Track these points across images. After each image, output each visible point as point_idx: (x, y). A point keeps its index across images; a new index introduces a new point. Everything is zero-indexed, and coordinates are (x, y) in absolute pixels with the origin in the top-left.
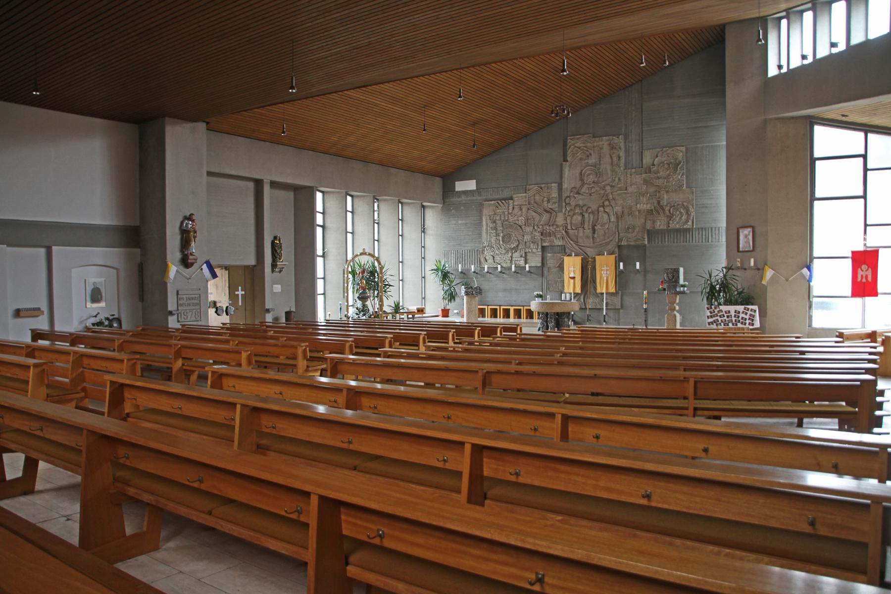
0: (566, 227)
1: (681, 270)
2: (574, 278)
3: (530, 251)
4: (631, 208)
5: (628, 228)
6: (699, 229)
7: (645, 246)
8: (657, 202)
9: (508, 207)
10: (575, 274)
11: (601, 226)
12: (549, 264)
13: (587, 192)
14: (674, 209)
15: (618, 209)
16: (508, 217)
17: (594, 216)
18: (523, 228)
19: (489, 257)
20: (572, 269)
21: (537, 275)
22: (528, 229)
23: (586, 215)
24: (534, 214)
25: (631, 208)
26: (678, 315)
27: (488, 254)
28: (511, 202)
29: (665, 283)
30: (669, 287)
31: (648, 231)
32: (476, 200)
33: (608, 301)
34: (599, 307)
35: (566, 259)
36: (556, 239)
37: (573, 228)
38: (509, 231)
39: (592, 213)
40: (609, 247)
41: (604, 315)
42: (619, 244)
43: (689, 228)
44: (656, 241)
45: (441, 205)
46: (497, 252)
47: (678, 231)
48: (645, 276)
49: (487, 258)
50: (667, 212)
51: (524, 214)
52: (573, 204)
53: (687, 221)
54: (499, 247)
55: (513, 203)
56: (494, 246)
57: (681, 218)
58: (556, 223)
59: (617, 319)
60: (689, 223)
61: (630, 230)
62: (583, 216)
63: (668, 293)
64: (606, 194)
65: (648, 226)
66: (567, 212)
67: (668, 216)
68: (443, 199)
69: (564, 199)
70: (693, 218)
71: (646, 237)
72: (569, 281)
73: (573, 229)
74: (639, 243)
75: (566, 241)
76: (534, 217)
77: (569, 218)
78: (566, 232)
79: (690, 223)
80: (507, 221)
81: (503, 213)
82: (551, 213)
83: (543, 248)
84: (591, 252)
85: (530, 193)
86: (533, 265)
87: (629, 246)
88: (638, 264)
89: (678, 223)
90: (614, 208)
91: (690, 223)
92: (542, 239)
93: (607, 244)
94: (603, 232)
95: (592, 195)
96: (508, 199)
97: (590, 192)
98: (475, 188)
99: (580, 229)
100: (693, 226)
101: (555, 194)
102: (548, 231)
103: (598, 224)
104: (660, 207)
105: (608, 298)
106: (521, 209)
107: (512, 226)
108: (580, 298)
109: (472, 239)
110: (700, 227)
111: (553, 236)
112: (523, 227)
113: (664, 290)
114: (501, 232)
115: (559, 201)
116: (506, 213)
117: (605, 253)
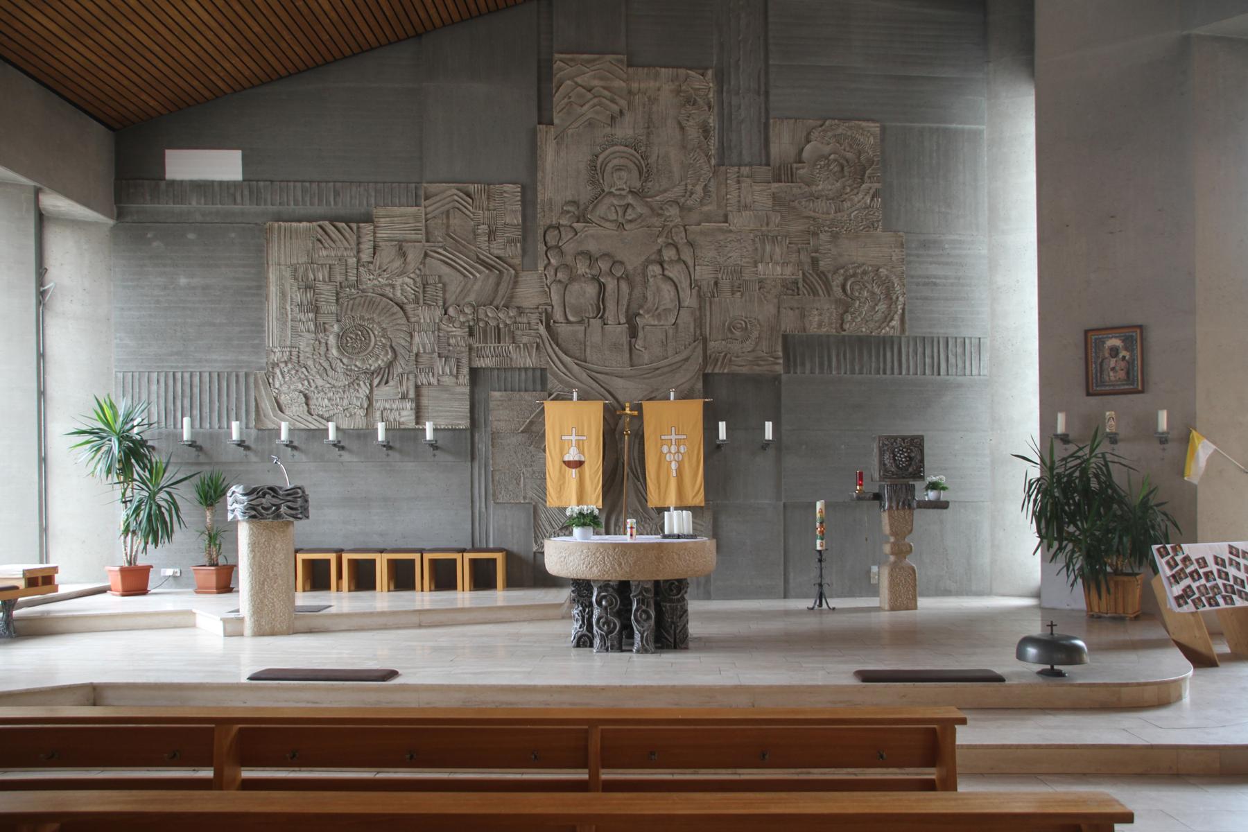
2: (579, 464)
3: (434, 381)
6: (915, 339)
10: (581, 452)
17: (632, 287)
18: (410, 313)
22: (425, 315)
24: (445, 270)
25: (739, 271)
28: (367, 228)
31: (785, 338)
37: (571, 319)
38: (362, 318)
44: (808, 366)
47: (862, 342)
49: (283, 399)
50: (837, 291)
51: (411, 267)
52: (569, 248)
53: (887, 318)
54: (326, 365)
56: (310, 363)
60: (893, 323)
65: (789, 323)
72: (562, 476)
73: (568, 322)
76: (445, 279)
84: (626, 390)
87: (733, 377)
90: (692, 270)
92: (471, 349)
100: (903, 330)
102: (493, 323)
104: (817, 275)
112: (409, 307)
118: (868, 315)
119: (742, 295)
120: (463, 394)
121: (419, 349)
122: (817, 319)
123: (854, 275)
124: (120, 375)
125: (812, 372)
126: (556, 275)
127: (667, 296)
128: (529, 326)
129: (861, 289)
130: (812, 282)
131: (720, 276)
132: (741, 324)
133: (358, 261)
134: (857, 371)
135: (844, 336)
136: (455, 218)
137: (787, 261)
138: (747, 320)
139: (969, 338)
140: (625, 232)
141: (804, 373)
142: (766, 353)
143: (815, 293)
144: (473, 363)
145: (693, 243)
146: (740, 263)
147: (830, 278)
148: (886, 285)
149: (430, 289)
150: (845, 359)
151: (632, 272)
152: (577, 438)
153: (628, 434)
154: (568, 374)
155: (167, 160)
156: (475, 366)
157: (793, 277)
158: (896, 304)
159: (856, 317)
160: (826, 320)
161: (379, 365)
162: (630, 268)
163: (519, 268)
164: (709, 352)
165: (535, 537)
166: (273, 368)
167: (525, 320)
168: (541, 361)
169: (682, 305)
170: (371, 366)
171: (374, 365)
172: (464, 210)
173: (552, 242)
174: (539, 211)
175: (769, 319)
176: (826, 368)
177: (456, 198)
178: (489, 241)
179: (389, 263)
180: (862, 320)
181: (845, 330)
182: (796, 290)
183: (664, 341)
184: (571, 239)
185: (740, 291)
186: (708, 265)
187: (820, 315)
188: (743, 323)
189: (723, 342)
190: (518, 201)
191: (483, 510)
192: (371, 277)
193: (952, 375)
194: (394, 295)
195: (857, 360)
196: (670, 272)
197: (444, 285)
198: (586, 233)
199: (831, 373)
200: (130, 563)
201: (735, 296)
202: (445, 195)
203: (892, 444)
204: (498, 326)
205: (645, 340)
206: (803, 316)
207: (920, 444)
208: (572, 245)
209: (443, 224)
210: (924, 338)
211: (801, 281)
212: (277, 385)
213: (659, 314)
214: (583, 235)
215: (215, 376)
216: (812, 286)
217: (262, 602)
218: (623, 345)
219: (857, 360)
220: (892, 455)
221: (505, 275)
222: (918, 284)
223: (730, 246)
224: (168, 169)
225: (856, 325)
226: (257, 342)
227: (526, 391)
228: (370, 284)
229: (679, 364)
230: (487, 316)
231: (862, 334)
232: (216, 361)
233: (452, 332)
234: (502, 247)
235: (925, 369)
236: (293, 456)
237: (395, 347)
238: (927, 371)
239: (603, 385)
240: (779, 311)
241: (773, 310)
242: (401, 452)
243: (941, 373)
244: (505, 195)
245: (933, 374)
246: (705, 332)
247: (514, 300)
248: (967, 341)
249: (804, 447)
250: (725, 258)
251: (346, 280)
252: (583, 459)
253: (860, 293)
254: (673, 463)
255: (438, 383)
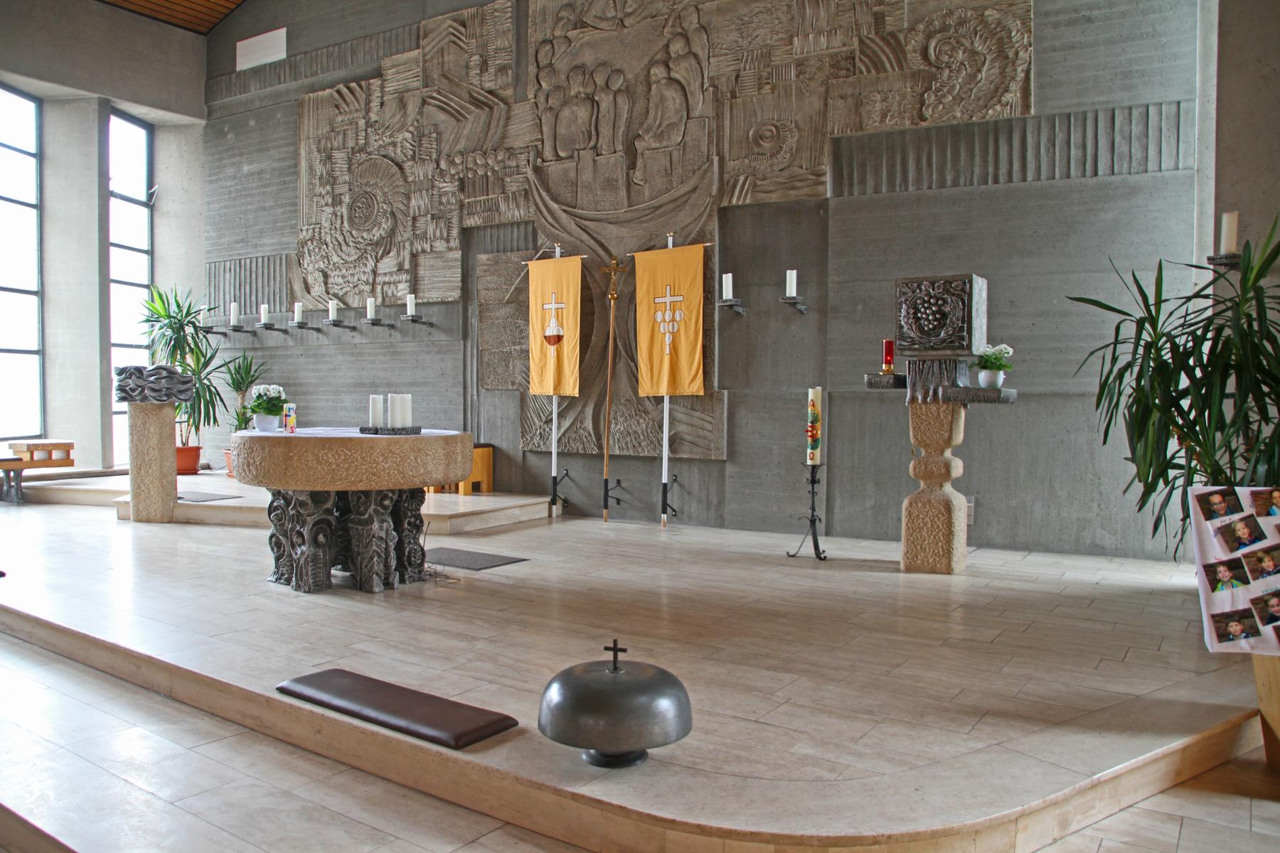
0: (539, 154)
1: (980, 287)
2: (559, 339)
3: (427, 247)
4: (766, 55)
5: (759, 137)
6: (1051, 119)
7: (823, 204)
8: (870, 19)
9: (368, 102)
10: (561, 325)
11: (659, 137)
12: (483, 293)
13: (611, 13)
14: (946, 41)
15: (720, 66)
16: (366, 137)
17: (633, 102)
18: (408, 171)
19: (315, 280)
20: (553, 306)
21: (448, 331)
22: (418, 172)
23: (605, 101)
24: (442, 117)
25: (766, 55)
26: (961, 505)
27: (312, 265)
28: (376, 83)
29: (903, 349)
30: (920, 368)
31: (836, 143)
32: (287, 92)
33: (682, 428)
34: (653, 454)
35: (535, 267)
36: (507, 199)
37: (562, 154)
38: (367, 184)
39: (628, 91)
40: (685, 217)
41: (665, 485)
42: (725, 204)
43: (1010, 121)
44: (870, 182)
45: (203, 122)
46: (335, 259)
47: (958, 134)
48: (823, 328)
49: (310, 280)
50: (915, 61)
51: (410, 120)
52: (562, 64)
53: (999, 90)
54: (341, 239)
55: (382, 87)
56: (328, 239)
57: (972, 78)
58: (510, 142)
59: (715, 501)
60: (1008, 97)
61: (766, 145)
62: (595, 104)
63: (914, 399)
64: (675, 14)
65: (837, 124)
66: (542, 99)
67: (915, 75)
68: (206, 102)
69: (531, 51)
70: (1027, 72)
71: (827, 168)
72: (543, 353)
73: (558, 158)
74: (802, 192)
75: (536, 205)
76: (442, 127)
77: (547, 119)
78: (537, 170)
79: (1014, 96)
80: (361, 150)
81: (353, 122)
82: (491, 108)
83: (467, 234)
84: (619, 239)
85: (429, 45)
86: (434, 296)
87: (760, 209)
88: (792, 276)
89: (958, 99)
90: (705, 64)
91: (1014, 96)
92: (462, 206)
93: (680, 203)
94: (664, 162)
95: (627, 23)
96: (367, 77)
97: (620, 15)
98: (283, 55)
99: (582, 152)
100: (1026, 106)
101: (502, 42)
102: (481, 172)
103: (648, 131)
104: (883, 39)
105: (679, 416)
106: (402, 104)
107: (376, 165)
108: (579, 419)
109: (275, 222)
110: (1073, 110)
111: (498, 191)
112: (408, 165)
113: (900, 382)
114: (345, 188)
115: (518, 63)
116: (362, 123)
117: (670, 240)
118: (964, 90)
119: (773, 89)
120: (455, 260)
121: (415, 212)
122: (878, 106)
123: (944, 28)
124: (208, 265)
125: (877, 190)
126: (547, 102)
127: (671, 107)
128: (518, 170)
129: (953, 49)
130: (874, 52)
131: (742, 65)
132: (771, 131)
133: (367, 123)
134: (949, 183)
135: (928, 129)
136: (449, 54)
137: (836, 26)
138: (778, 124)
139: (1155, 104)
140: (626, 31)
141: (864, 193)
142: (806, 169)
143: (879, 67)
144: (464, 223)
145: (707, 26)
146: (769, 42)
147: (902, 40)
148: (998, 36)
149: (425, 141)
150: (930, 165)
151: (633, 81)
152: (556, 306)
153: (613, 298)
154: (555, 224)
155: (239, 53)
156: (465, 226)
157: (844, 49)
158: (1013, 65)
159: (944, 96)
160: (895, 107)
161: (381, 235)
162: (630, 76)
163: (511, 100)
164: (726, 177)
165: (522, 432)
166: (303, 247)
167: (514, 164)
168: (529, 212)
169: (692, 115)
170: (374, 236)
171: (377, 234)
172: (458, 42)
173: (544, 61)
174: (530, 24)
175: (811, 117)
176: (898, 182)
177: (451, 30)
178: (481, 75)
179: (391, 118)
180: (954, 98)
181: (925, 120)
182: (852, 69)
183: (669, 168)
184: (564, 52)
185: (768, 83)
186: (726, 54)
187: (884, 100)
188: (773, 129)
189: (746, 160)
190: (508, 18)
191: (475, 397)
192: (377, 137)
193: (1120, 174)
194: (395, 153)
195: (949, 166)
196: (677, 72)
197: (439, 134)
198: (581, 42)
199: (906, 189)
200: (184, 444)
201: (763, 91)
202: (441, 29)
203: (914, 292)
204: (486, 175)
205: (645, 171)
206: (859, 104)
207: (963, 290)
208: (565, 60)
209: (438, 63)
210: (1069, 115)
211: (858, 53)
212: (306, 266)
213: (662, 132)
214: (578, 45)
215: (266, 259)
216: (875, 59)
217: (139, 487)
218: (617, 181)
219: (949, 166)
220: (912, 311)
221: (496, 110)
222: (1056, 25)
223: (756, 21)
224: (239, 60)
225: (943, 107)
226: (293, 222)
227: (512, 251)
228: (376, 145)
229: (686, 198)
230: (476, 164)
231: (955, 122)
232: (266, 245)
233: (443, 188)
234: (493, 78)
235: (1069, 168)
236: (318, 339)
237: (396, 213)
238: (1073, 172)
239: (595, 236)
240: (826, 105)
241: (817, 104)
242: (401, 331)
243: (1100, 173)
244: (496, 14)
245: (1084, 176)
246: (723, 149)
247: (506, 140)
248: (1152, 111)
249: (860, 307)
250: (750, 39)
251: (357, 144)
252: (561, 334)
253: (950, 57)
254: (667, 335)
255: (431, 250)
